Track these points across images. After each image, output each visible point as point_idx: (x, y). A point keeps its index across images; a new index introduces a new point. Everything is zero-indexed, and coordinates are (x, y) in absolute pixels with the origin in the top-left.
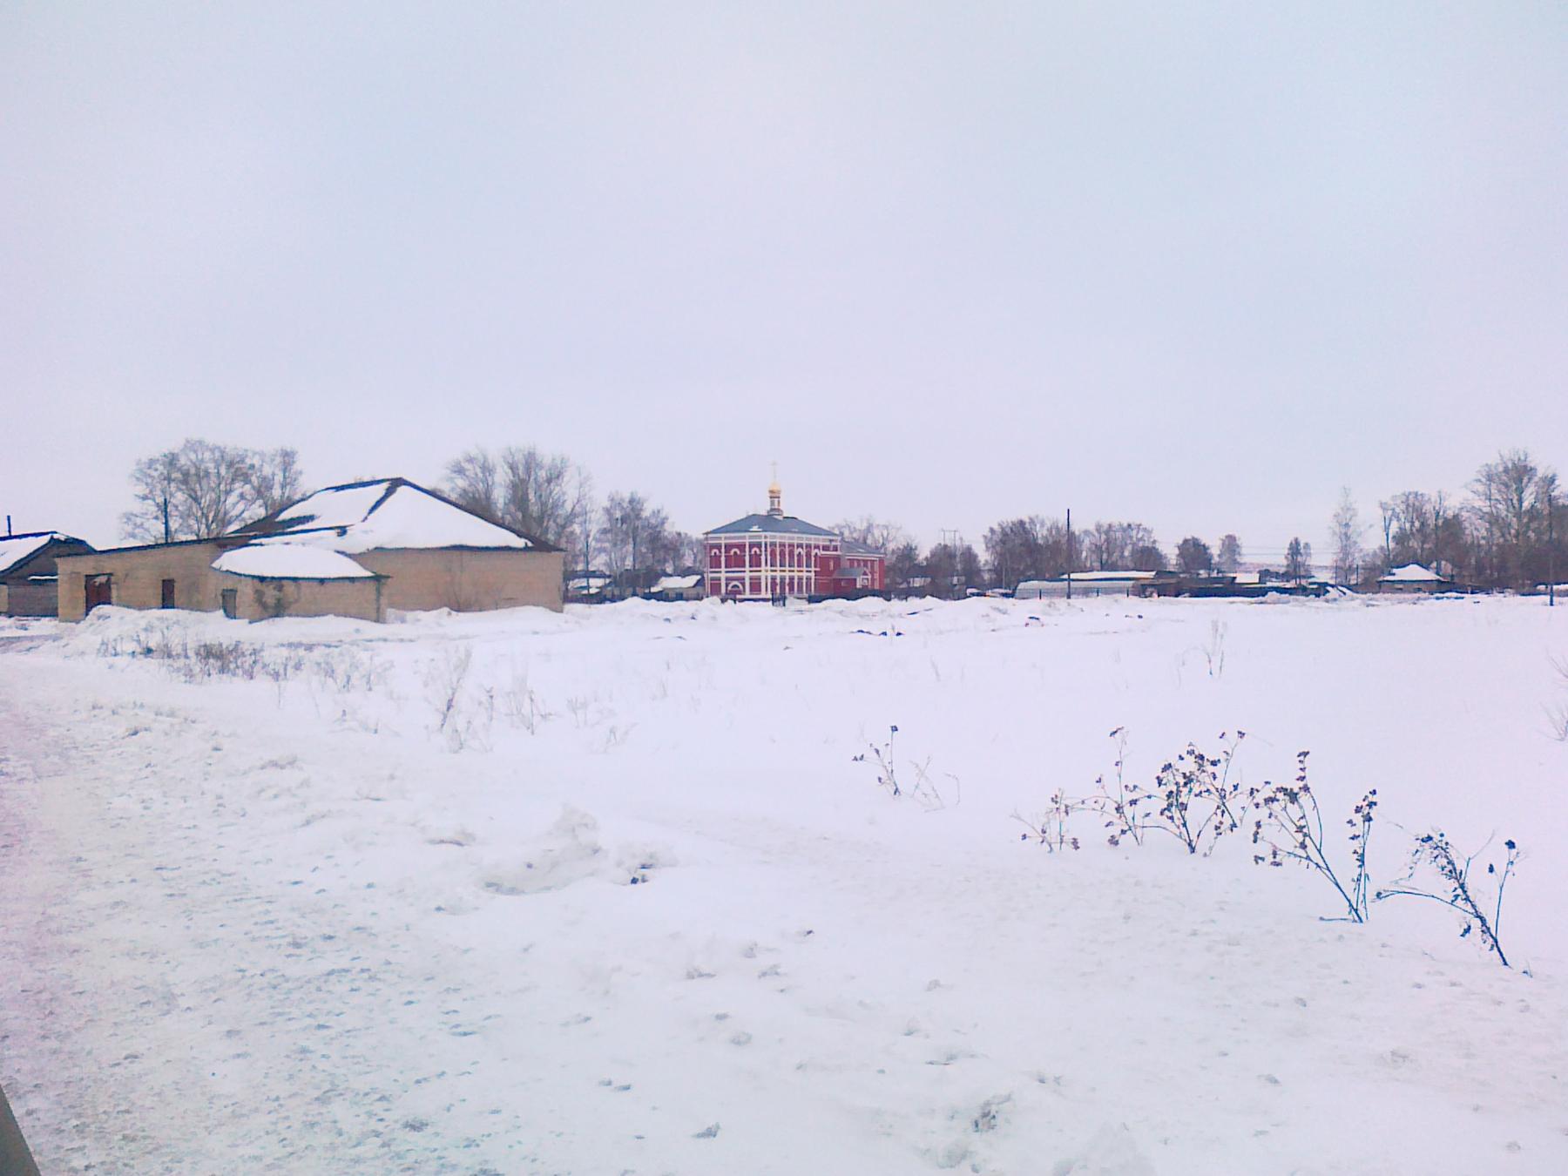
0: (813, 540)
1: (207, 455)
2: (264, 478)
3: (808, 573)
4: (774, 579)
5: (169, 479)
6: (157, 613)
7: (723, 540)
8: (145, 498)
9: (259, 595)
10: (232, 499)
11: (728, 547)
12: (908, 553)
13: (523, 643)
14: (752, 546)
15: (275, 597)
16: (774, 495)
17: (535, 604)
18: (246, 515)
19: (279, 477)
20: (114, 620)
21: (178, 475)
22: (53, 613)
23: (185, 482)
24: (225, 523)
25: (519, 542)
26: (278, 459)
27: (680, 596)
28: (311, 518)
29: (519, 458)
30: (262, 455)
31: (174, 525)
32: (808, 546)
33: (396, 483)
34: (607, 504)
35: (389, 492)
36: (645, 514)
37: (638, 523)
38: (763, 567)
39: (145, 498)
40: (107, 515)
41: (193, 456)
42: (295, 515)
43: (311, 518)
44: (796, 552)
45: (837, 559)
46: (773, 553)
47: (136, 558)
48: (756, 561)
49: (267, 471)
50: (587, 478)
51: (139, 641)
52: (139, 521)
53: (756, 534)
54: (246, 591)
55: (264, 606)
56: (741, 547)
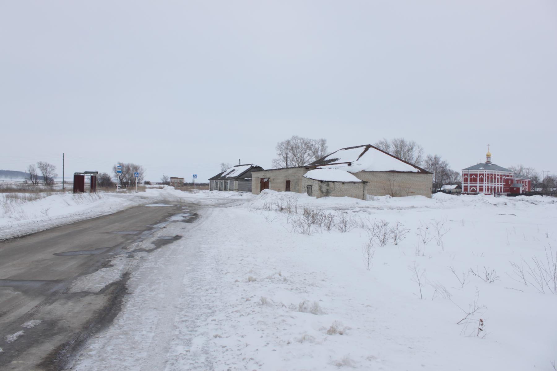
0: (503, 173)
1: (299, 141)
2: (316, 149)
3: (501, 185)
4: (488, 187)
5: (287, 149)
6: (284, 193)
7: (470, 172)
8: (280, 155)
9: (320, 187)
10: (306, 155)
11: (471, 175)
12: (535, 179)
13: (419, 212)
14: (480, 175)
15: (327, 189)
16: (488, 156)
17: (422, 195)
18: (310, 160)
19: (320, 148)
20: (270, 195)
21: (290, 148)
22: (250, 190)
23: (292, 149)
24: (303, 163)
25: (416, 170)
26: (320, 142)
27: (450, 192)
28: (336, 159)
29: (398, 142)
30: (315, 141)
31: (288, 164)
32: (501, 175)
33: (368, 147)
34: (427, 159)
35: (366, 150)
36: (440, 163)
37: (438, 166)
38: (484, 182)
39: (280, 155)
40: (269, 159)
41: (294, 141)
42: (331, 158)
43: (336, 159)
44: (497, 177)
45: (512, 181)
46: (488, 178)
47: (277, 173)
48: (481, 180)
49: (317, 146)
50: (422, 149)
51: (278, 206)
52: (278, 162)
53: (482, 170)
54: (316, 186)
55: (322, 192)
56: (476, 175)
